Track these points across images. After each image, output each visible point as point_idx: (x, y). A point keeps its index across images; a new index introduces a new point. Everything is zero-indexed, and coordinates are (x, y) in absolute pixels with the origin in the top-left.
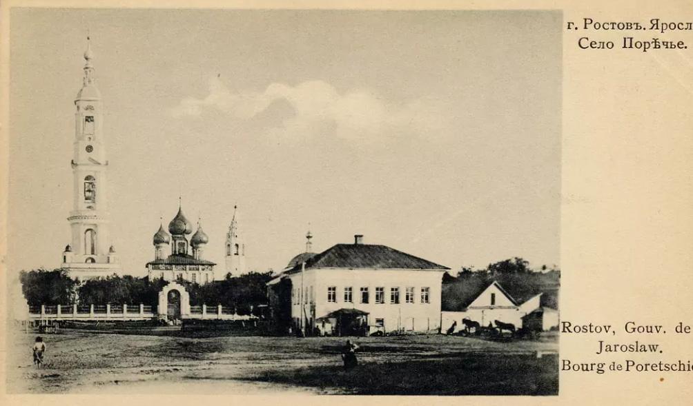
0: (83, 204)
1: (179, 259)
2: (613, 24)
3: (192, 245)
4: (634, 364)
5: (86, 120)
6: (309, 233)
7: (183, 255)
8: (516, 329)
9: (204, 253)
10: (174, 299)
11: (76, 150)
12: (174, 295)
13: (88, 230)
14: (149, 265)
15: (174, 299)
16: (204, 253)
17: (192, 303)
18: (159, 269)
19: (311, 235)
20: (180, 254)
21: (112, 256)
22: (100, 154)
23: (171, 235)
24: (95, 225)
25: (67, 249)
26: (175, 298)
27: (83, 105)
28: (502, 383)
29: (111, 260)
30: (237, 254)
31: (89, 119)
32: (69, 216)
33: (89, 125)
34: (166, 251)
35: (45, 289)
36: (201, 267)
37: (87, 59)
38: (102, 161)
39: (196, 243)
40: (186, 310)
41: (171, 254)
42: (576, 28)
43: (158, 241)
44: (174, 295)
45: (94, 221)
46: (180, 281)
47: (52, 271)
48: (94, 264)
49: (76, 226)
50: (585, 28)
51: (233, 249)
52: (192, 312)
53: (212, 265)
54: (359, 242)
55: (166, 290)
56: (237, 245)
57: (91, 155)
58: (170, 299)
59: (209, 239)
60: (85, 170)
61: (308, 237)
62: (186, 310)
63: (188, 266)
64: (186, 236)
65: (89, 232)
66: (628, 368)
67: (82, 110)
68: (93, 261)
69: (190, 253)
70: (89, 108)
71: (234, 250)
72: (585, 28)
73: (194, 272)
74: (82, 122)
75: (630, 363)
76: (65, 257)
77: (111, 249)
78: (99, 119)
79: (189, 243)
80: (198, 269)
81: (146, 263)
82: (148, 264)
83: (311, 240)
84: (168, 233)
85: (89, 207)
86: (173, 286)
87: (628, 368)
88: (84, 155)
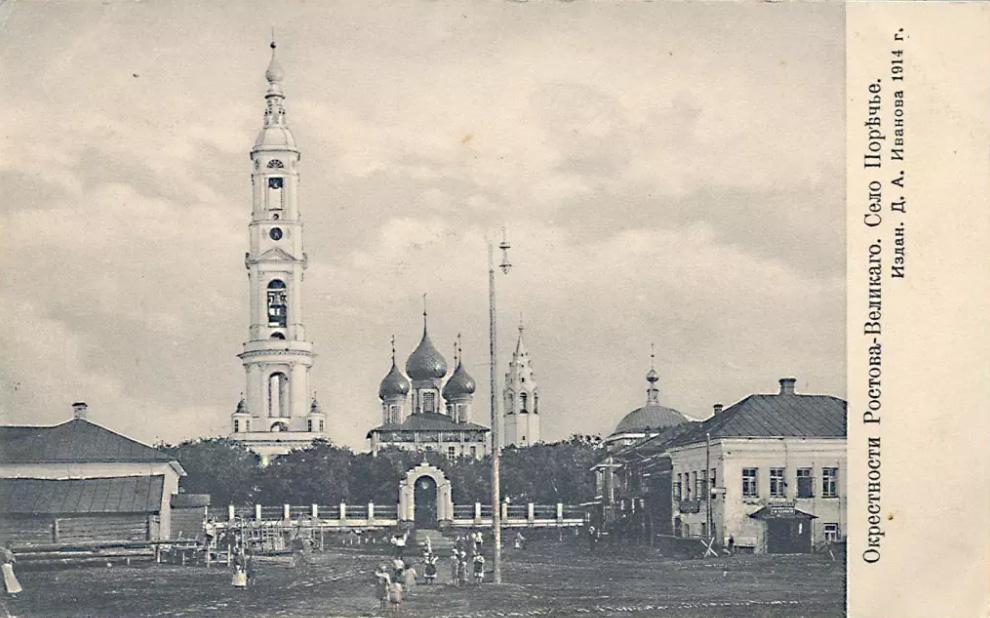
2: (870, 454)
3: (445, 396)
4: (868, 413)
5: (271, 186)
7: (432, 415)
9: (475, 411)
10: (426, 494)
12: (425, 486)
13: (272, 375)
14: (375, 434)
15: (426, 494)
16: (475, 411)
19: (655, 376)
23: (410, 380)
30: (524, 411)
31: (277, 183)
33: (276, 193)
34: (404, 409)
36: (463, 436)
37: (270, 80)
38: (299, 256)
39: (457, 391)
40: (445, 508)
41: (410, 414)
42: (901, 30)
43: (389, 391)
44: (425, 486)
45: (286, 358)
46: (438, 460)
47: (340, 446)
48: (283, 434)
50: (878, 421)
55: (413, 475)
56: (524, 397)
59: (477, 386)
60: (273, 270)
61: (652, 380)
62: (445, 508)
63: (441, 435)
64: (436, 382)
65: (276, 378)
66: (875, 421)
67: (264, 167)
69: (444, 411)
71: (519, 404)
72: (878, 421)
73: (451, 444)
74: (263, 189)
75: (868, 417)
76: (237, 421)
77: (240, 406)
78: (291, 182)
79: (441, 392)
80: (457, 440)
81: (369, 430)
82: (373, 431)
83: (656, 385)
84: (405, 375)
85: (275, 335)
86: (425, 469)
87: (875, 421)
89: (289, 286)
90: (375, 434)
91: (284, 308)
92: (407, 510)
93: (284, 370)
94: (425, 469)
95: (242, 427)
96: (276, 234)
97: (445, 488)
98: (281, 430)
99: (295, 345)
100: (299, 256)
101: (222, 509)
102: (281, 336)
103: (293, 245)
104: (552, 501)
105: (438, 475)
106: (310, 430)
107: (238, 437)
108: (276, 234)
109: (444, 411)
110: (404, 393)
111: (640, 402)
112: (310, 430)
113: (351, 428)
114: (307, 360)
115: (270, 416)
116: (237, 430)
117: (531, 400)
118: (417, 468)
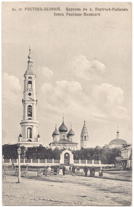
0: (27, 117)
1: (64, 142)
3: (67, 136)
6: (118, 131)
8: (53, 150)
10: (67, 157)
11: (25, 95)
12: (67, 155)
15: (67, 157)
17: (74, 159)
18: (55, 145)
19: (119, 132)
20: (63, 140)
21: (39, 139)
22: (34, 97)
24: (32, 126)
25: (20, 136)
26: (68, 157)
27: (28, 76)
28: (100, 165)
29: (39, 140)
32: (21, 122)
33: (30, 85)
35: (10, 152)
40: (72, 161)
44: (67, 155)
48: (31, 142)
49: (24, 126)
51: (84, 137)
52: (74, 163)
53: (76, 144)
54: (118, 138)
55: (64, 153)
57: (31, 97)
58: (65, 157)
62: (72, 161)
67: (27, 78)
68: (30, 141)
69: (67, 139)
70: (30, 78)
76: (19, 139)
83: (119, 134)
86: (67, 151)
88: (28, 96)
89: (33, 107)
90: (51, 144)
91: (31, 113)
92: (62, 161)
93: (31, 127)
94: (67, 151)
95: (20, 140)
96: (30, 94)
97: (72, 156)
98: (30, 141)
99: (34, 121)
100: (35, 100)
101: (15, 160)
102: (30, 119)
103: (34, 97)
104: (78, 159)
105: (70, 153)
106: (37, 141)
107: (20, 143)
108: (30, 94)
109: (67, 139)
110: (58, 135)
111: (115, 138)
112: (37, 141)
113: (46, 142)
114: (37, 125)
115: (27, 138)
116: (19, 141)
117: (87, 137)
118: (65, 151)
